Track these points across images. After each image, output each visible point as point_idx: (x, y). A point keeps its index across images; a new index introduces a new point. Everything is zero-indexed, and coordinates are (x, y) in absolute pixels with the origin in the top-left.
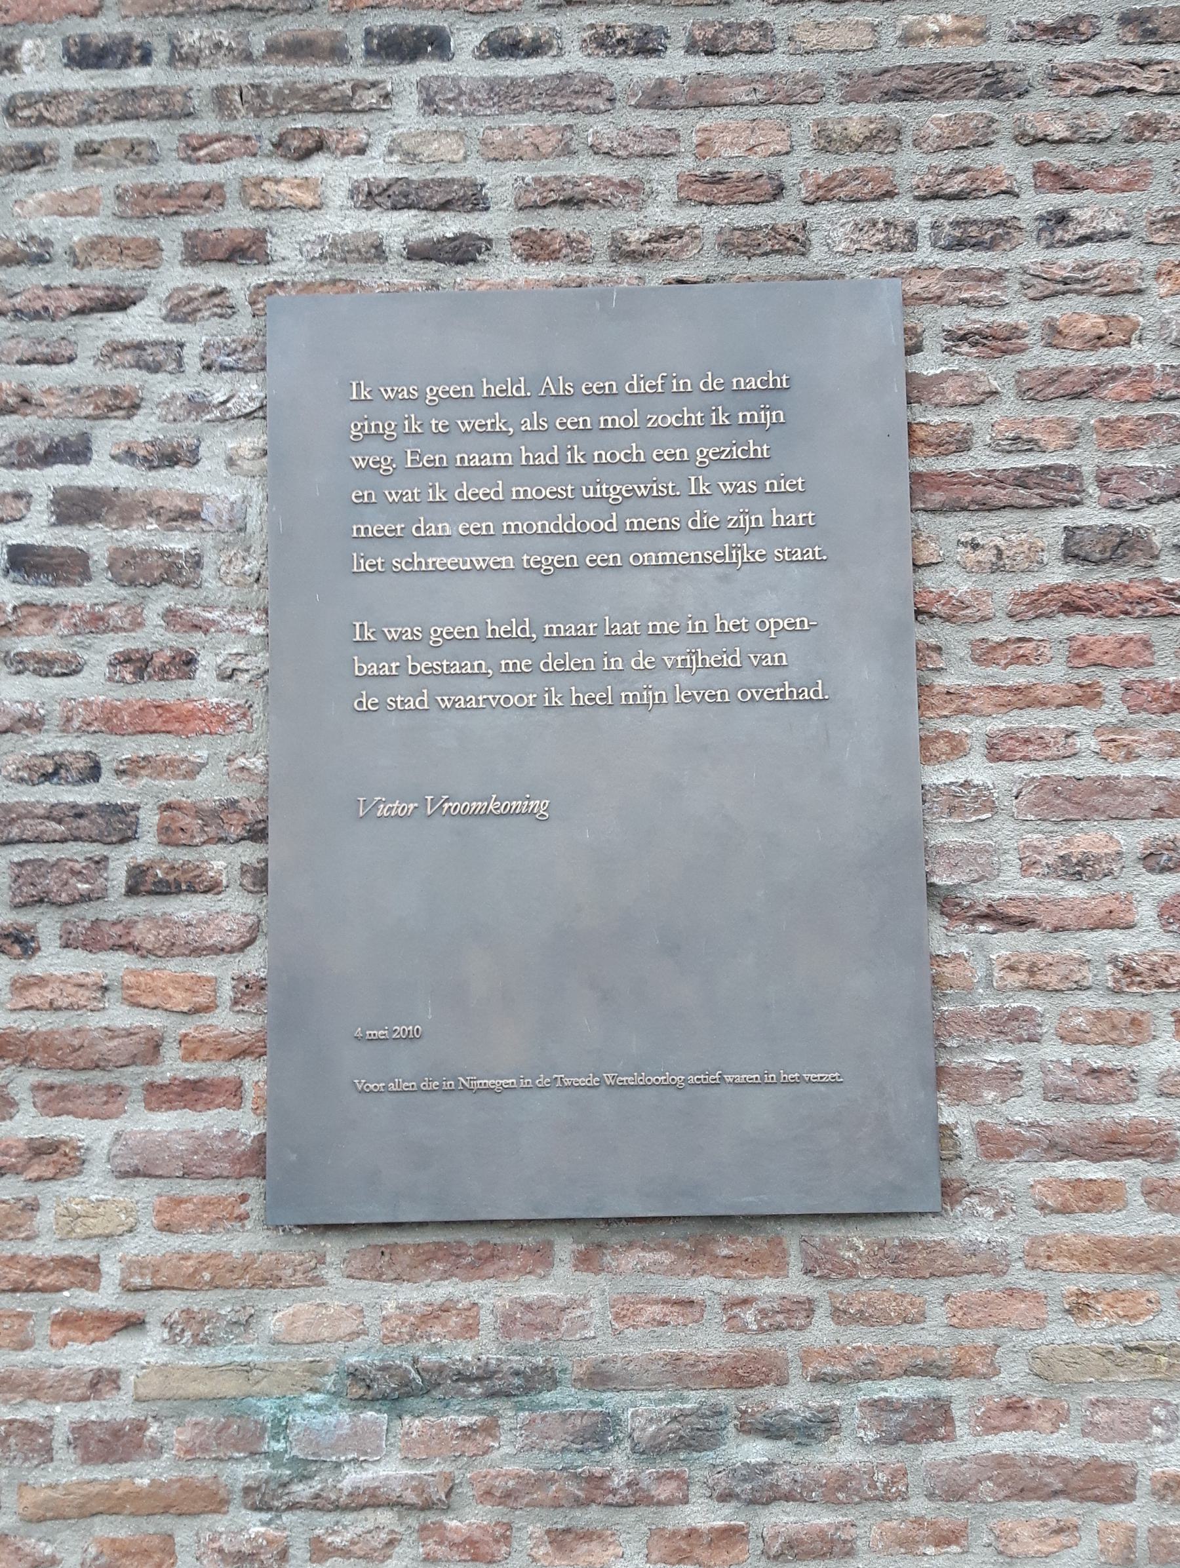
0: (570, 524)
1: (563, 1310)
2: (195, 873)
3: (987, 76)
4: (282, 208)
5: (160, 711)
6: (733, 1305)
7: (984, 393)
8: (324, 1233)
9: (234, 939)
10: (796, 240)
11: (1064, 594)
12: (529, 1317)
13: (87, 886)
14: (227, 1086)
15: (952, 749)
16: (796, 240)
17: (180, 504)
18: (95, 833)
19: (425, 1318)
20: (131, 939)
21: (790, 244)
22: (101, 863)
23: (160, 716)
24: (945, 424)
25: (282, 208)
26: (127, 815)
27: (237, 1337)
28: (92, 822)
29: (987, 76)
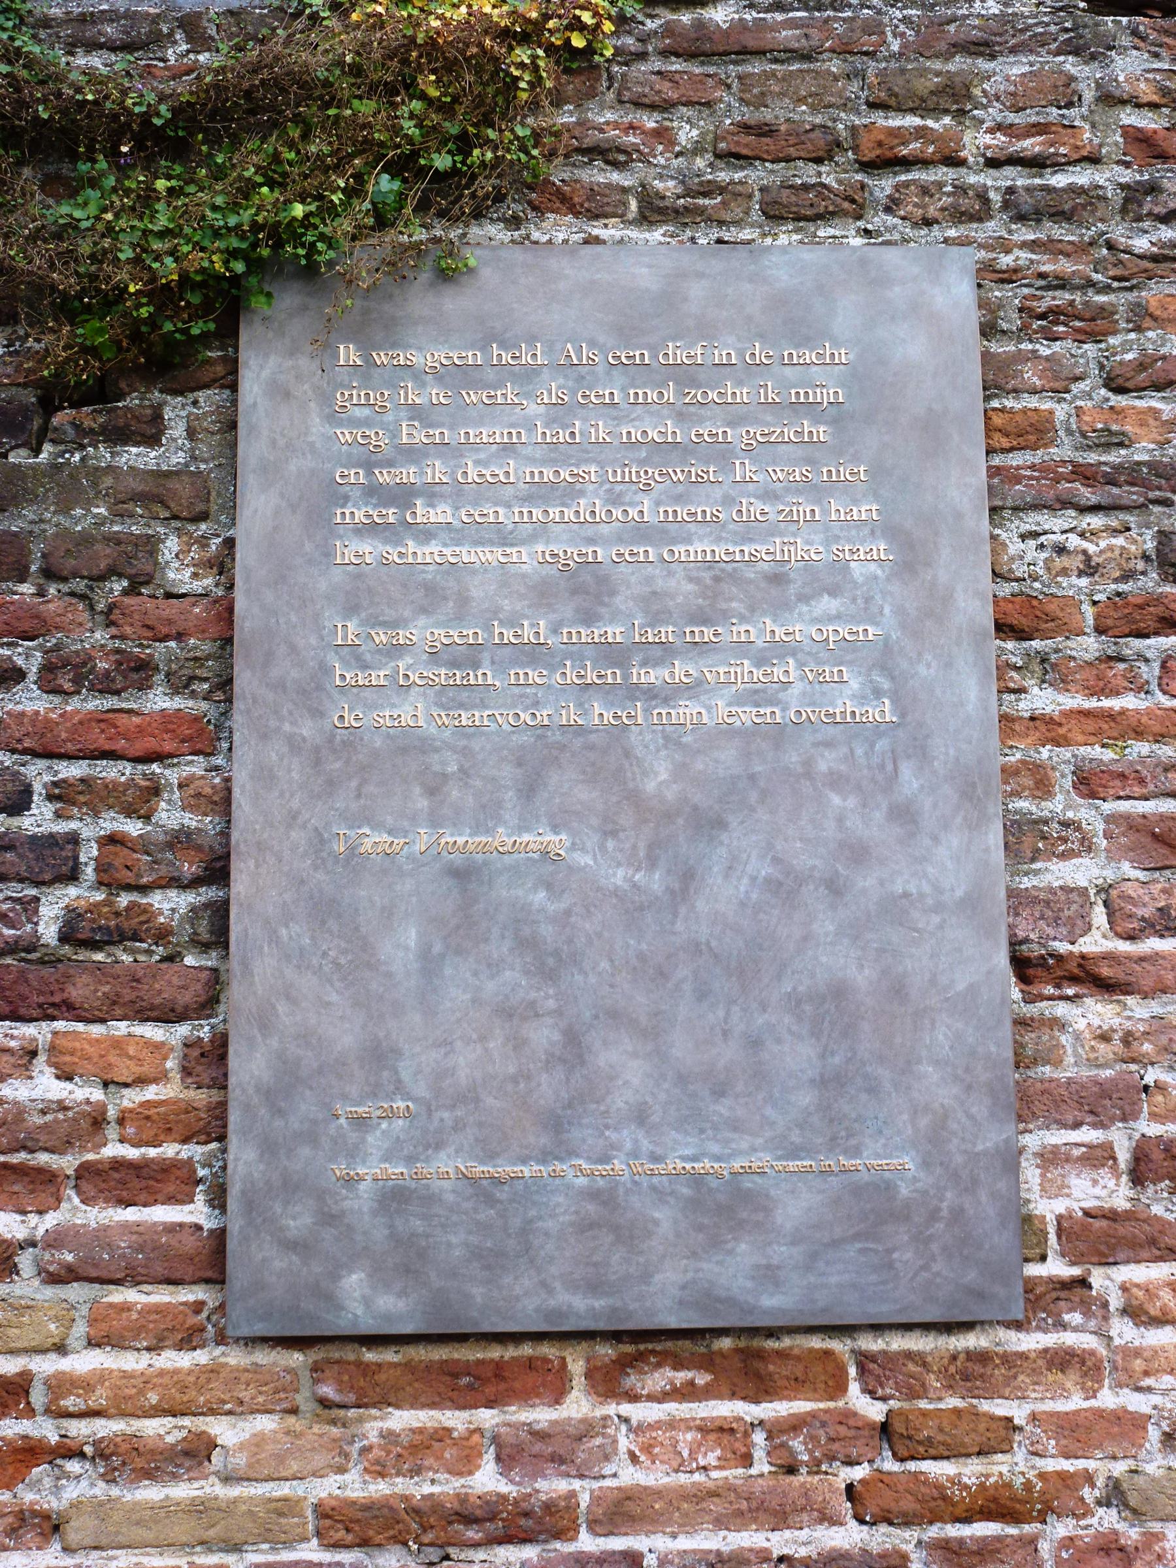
0: (573, 433)
1: (580, 1439)
2: (142, 918)
3: (1066, 30)
4: (740, 1353)
5: (103, 725)
6: (782, 1432)
7: (1068, 379)
8: (273, 1347)
9: (186, 998)
10: (853, 201)
11: (1161, 608)
12: (538, 1447)
13: (13, 932)
14: (178, 1173)
15: (1036, 783)
16: (853, 201)
17: (133, 485)
18: (23, 870)
19: (414, 1448)
20: (66, 995)
21: (846, 205)
22: (31, 906)
23: (103, 731)
24: (1025, 411)
25: (740, 1353)
26: (62, 849)
27: (189, 1470)
28: (20, 856)
29: (1066, 30)
